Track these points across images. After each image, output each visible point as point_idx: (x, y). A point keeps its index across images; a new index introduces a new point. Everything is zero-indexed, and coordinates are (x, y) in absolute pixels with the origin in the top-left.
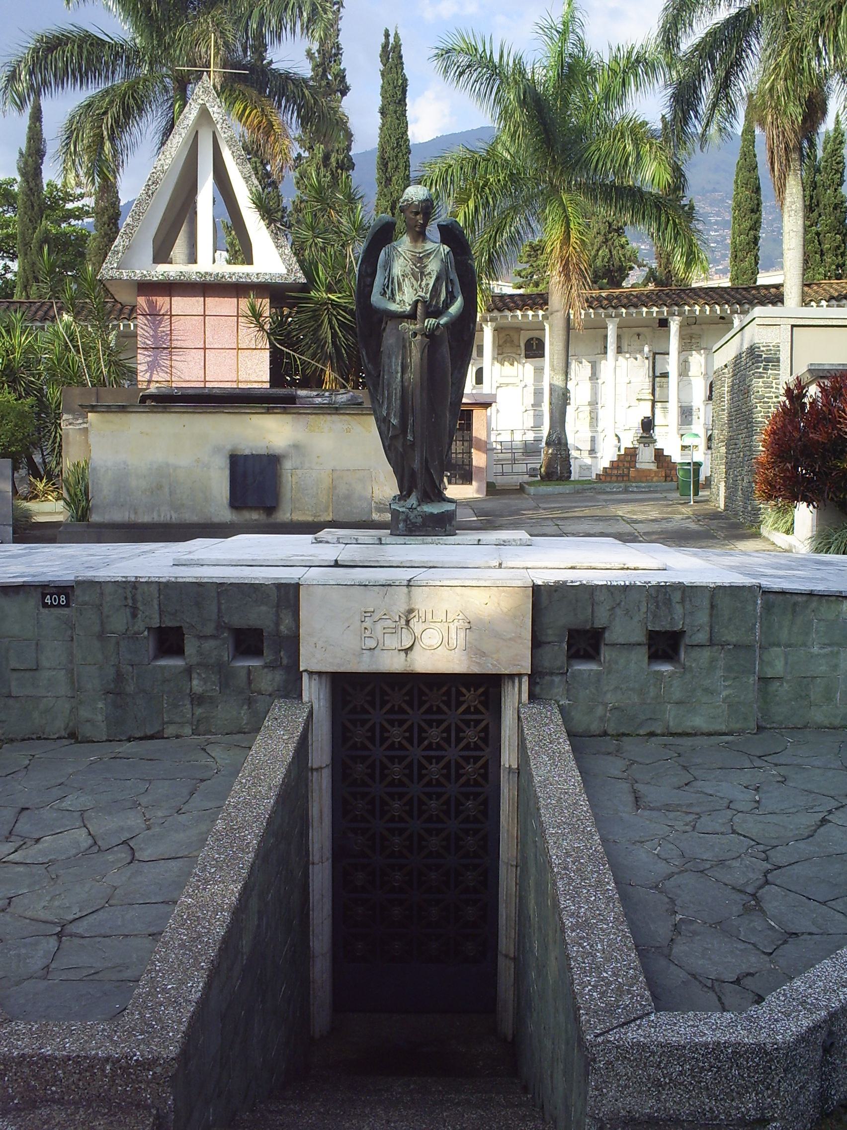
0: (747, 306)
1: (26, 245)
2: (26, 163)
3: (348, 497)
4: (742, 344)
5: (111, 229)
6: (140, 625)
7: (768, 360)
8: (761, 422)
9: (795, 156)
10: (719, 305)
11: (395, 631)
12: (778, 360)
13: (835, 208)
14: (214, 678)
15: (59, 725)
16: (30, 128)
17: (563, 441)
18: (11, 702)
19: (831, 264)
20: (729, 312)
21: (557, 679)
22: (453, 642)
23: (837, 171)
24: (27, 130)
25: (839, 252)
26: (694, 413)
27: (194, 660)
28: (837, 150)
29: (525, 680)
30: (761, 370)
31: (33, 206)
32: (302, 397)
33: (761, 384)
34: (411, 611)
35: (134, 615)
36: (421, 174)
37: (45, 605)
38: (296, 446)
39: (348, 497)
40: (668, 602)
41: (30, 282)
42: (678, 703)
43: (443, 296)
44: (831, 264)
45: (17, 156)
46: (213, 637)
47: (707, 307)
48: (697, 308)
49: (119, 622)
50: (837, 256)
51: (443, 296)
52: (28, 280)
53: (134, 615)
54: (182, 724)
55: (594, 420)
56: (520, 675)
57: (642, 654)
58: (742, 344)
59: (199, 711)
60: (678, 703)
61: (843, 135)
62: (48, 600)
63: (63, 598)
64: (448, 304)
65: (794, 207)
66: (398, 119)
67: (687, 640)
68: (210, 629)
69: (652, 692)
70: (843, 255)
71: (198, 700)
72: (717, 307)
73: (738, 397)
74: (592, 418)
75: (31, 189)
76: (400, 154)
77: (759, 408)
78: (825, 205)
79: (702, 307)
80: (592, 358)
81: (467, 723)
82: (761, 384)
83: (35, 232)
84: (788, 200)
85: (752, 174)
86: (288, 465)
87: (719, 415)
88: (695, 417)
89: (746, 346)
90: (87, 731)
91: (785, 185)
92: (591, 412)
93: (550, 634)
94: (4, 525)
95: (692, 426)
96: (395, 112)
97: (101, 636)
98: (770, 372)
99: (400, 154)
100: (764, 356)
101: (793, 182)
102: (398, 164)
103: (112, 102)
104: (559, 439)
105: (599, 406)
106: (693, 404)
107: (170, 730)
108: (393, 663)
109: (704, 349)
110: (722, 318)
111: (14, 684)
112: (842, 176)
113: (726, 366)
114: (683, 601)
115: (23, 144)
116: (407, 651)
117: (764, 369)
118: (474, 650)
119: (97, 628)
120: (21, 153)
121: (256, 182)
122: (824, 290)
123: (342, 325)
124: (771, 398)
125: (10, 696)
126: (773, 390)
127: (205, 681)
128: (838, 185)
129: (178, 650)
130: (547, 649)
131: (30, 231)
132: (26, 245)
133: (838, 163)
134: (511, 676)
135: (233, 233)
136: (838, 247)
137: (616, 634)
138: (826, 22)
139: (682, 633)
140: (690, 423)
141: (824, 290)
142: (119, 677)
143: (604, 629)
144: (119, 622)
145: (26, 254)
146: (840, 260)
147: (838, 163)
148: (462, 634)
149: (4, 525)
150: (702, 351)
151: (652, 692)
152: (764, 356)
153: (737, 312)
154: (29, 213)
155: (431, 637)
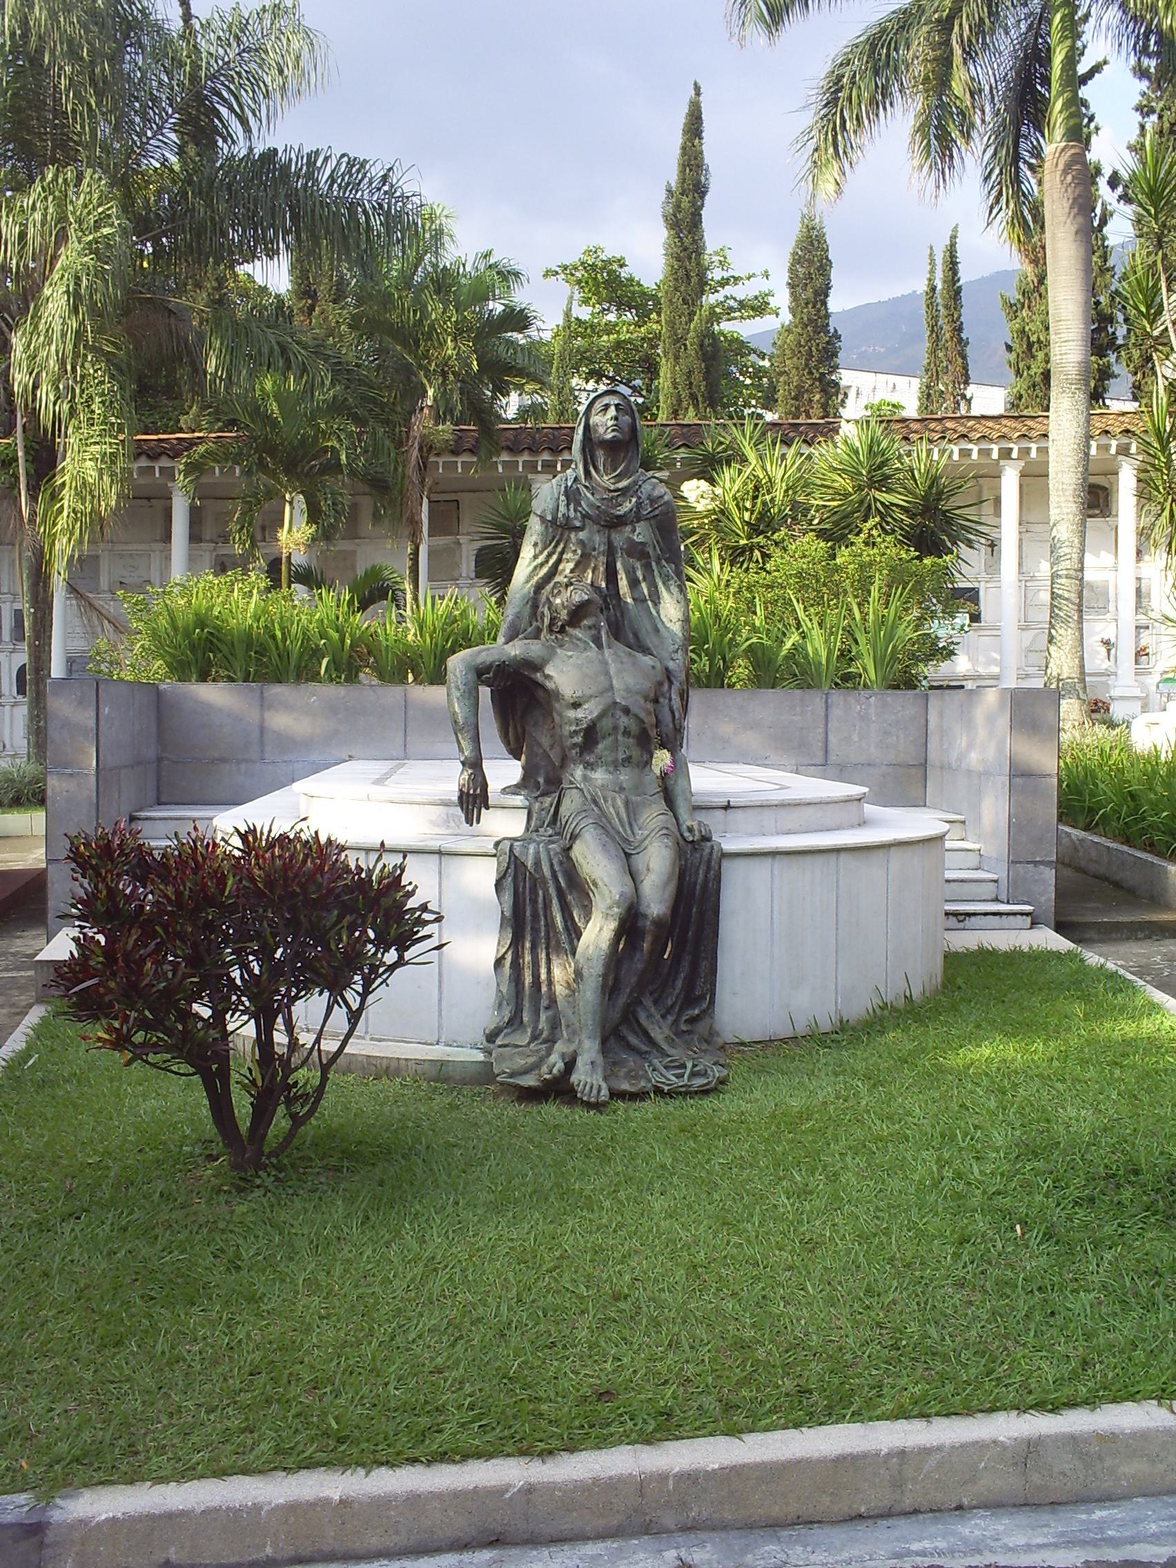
1: (678, 340)
2: (678, 207)
5: (819, 311)
16: (684, 148)
24: (678, 151)
31: (688, 277)
41: (685, 404)
45: (663, 195)
52: (680, 401)
83: (691, 320)
85: (741, 669)
94: (1035, 863)
115: (671, 174)
120: (669, 191)
131: (683, 319)
132: (678, 340)
135: (682, 548)
145: (677, 358)
149: (1035, 863)
154: (682, 289)
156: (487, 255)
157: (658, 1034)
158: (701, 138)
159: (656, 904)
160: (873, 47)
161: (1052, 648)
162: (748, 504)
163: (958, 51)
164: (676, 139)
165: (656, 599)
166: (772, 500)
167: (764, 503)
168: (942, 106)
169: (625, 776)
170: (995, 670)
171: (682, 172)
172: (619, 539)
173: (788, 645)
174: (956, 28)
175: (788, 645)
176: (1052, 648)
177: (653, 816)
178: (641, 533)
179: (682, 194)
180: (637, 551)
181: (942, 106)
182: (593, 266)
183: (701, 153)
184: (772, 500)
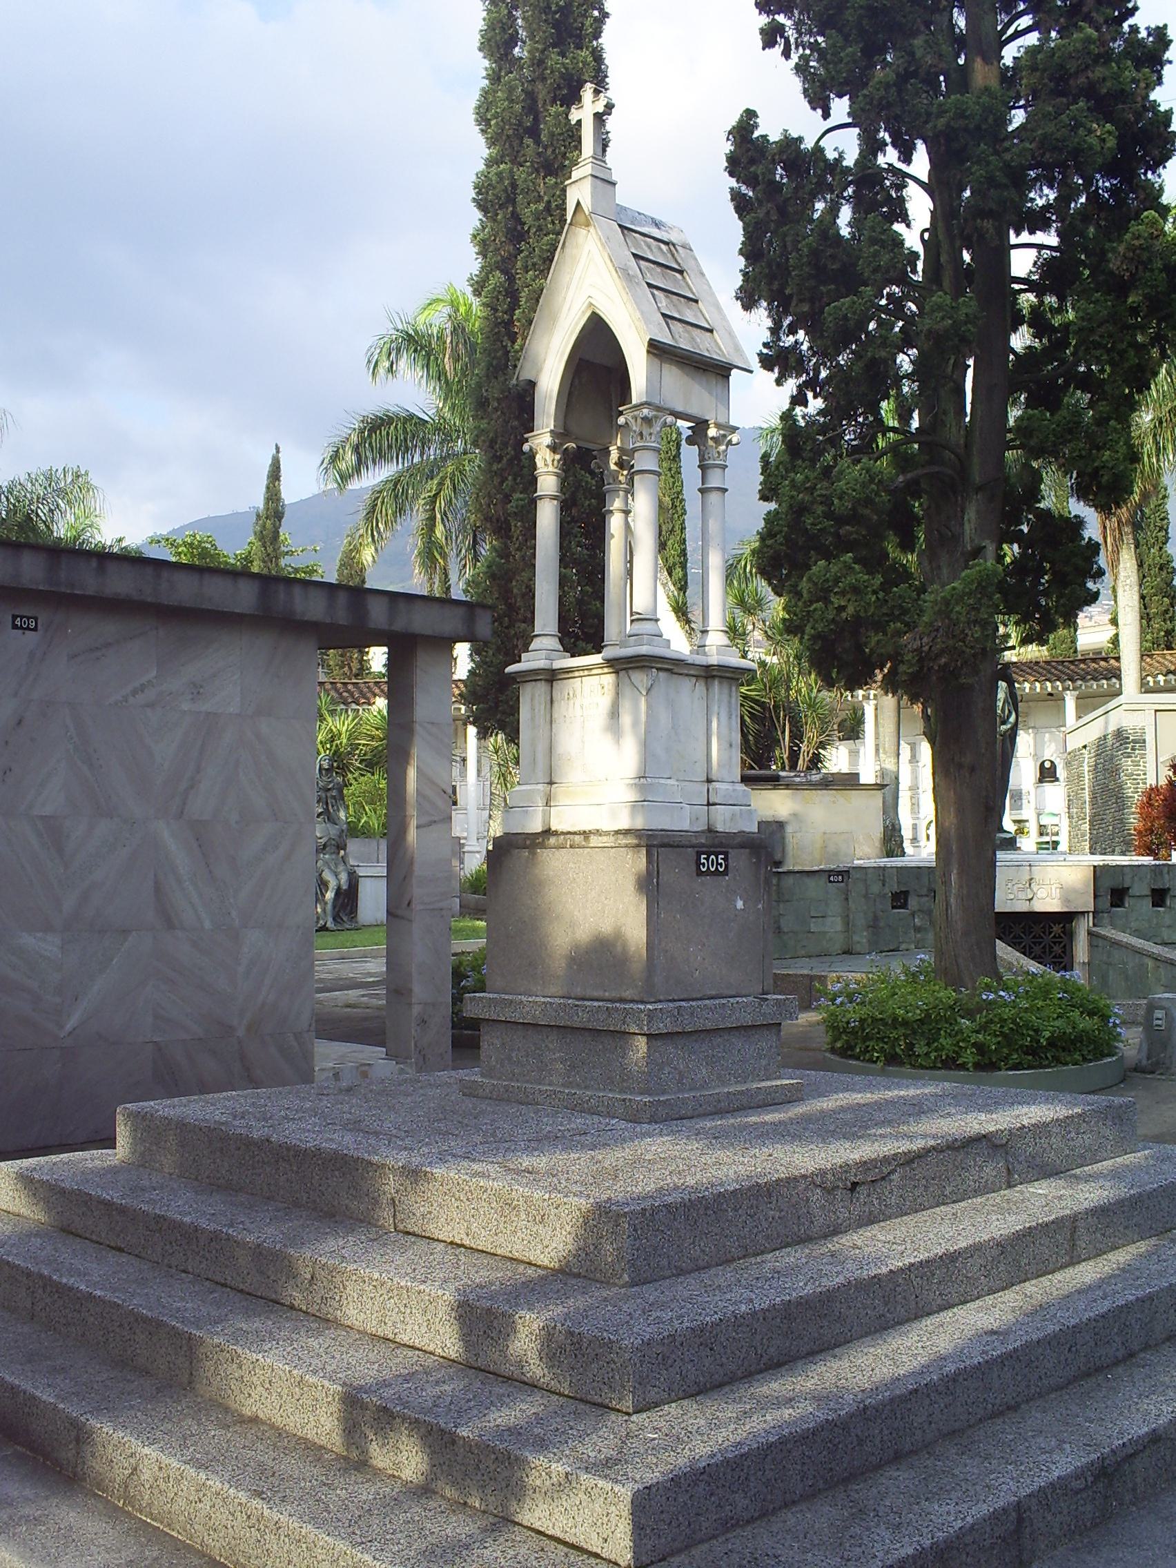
0: (1079, 682)
2: (264, 526)
3: (836, 854)
4: (1106, 728)
6: (887, 890)
7: (1134, 741)
8: (1131, 797)
9: (1127, 529)
10: (1050, 682)
11: (1023, 890)
12: (1144, 741)
13: (1161, 569)
14: (927, 917)
15: (837, 947)
16: (268, 488)
17: (897, 827)
18: (810, 935)
19: (1159, 630)
20: (1060, 689)
21: (1106, 915)
22: (1054, 896)
23: (1161, 529)
24: (264, 489)
25: (1167, 616)
26: (1024, 797)
27: (916, 908)
28: (1160, 505)
29: (1091, 914)
30: (1129, 750)
32: (784, 777)
33: (1130, 763)
34: (1031, 879)
35: (884, 885)
36: (742, 552)
37: (830, 882)
38: (795, 815)
39: (836, 854)
40: (1161, 873)
42: (1169, 927)
43: (1007, 712)
44: (1159, 630)
46: (927, 896)
47: (1038, 684)
48: (1027, 685)
49: (875, 888)
50: (1164, 620)
51: (1007, 712)
53: (884, 885)
54: (909, 943)
55: (916, 806)
56: (1088, 912)
57: (1149, 901)
58: (1106, 728)
59: (919, 936)
60: (1169, 927)
61: (1166, 489)
62: (832, 879)
63: (840, 877)
64: (1009, 717)
65: (1128, 582)
66: (672, 477)
67: (1172, 893)
68: (924, 891)
69: (1155, 921)
70: (1171, 619)
71: (918, 930)
72: (1048, 684)
73: (1104, 775)
74: (913, 804)
75: (268, 555)
76: (676, 516)
77: (1129, 785)
78: (1150, 565)
79: (1032, 683)
80: (911, 739)
81: (1055, 943)
82: (1130, 763)
84: (1122, 574)
86: (789, 829)
87: (1077, 794)
88: (1024, 802)
89: (1112, 728)
90: (858, 948)
91: (1118, 559)
92: (911, 798)
93: (1101, 892)
95: (1022, 812)
96: (670, 469)
97: (866, 896)
98: (1137, 752)
99: (676, 516)
100: (1131, 738)
101: (1126, 556)
102: (673, 527)
103: (441, 484)
104: (893, 825)
105: (920, 791)
106: (1022, 787)
107: (903, 946)
108: (1022, 907)
109: (1033, 728)
110: (1050, 694)
111: (812, 925)
112: (1167, 533)
113: (1085, 747)
114: (1168, 873)
116: (1030, 900)
117: (1132, 749)
118: (1066, 900)
119: (864, 892)
121: (672, 588)
122: (1158, 662)
123: (752, 716)
124: (1139, 775)
125: (810, 932)
126: (1141, 768)
127: (922, 919)
128: (1164, 544)
129: (904, 906)
130: (1100, 899)
133: (1162, 520)
134: (1083, 913)
136: (1166, 612)
137: (1135, 891)
138: (1164, 424)
139: (1169, 889)
140: (1020, 808)
141: (1158, 662)
142: (876, 919)
143: (1128, 888)
144: (875, 888)
146: (1169, 625)
147: (1162, 520)
148: (1058, 890)
150: (1030, 731)
151: (1155, 921)
152: (1131, 738)
153: (1068, 689)
155: (1041, 893)
156: (120, 540)
157: (345, 919)
158: (279, 481)
159: (345, 887)
160: (395, 485)
161: (491, 822)
162: (328, 746)
163: (438, 516)
164: (264, 482)
165: (339, 810)
166: (341, 743)
167: (337, 746)
168: (430, 542)
169: (334, 856)
170: (465, 834)
171: (267, 503)
172: (329, 795)
173: (363, 821)
174: (438, 504)
175: (363, 821)
176: (491, 822)
177: (341, 868)
178: (334, 793)
179: (267, 518)
180: (334, 797)
181: (430, 542)
182: (191, 544)
183: (279, 491)
184: (341, 743)
